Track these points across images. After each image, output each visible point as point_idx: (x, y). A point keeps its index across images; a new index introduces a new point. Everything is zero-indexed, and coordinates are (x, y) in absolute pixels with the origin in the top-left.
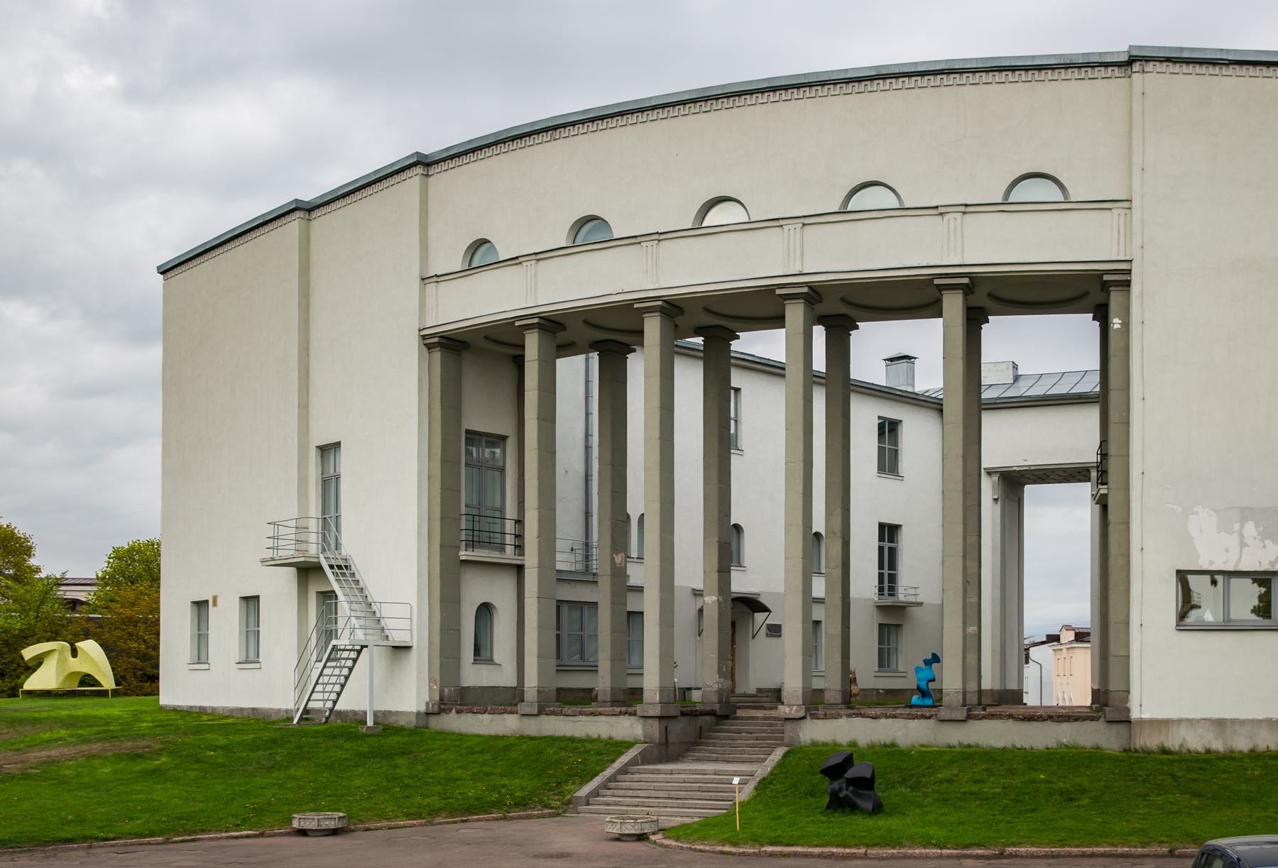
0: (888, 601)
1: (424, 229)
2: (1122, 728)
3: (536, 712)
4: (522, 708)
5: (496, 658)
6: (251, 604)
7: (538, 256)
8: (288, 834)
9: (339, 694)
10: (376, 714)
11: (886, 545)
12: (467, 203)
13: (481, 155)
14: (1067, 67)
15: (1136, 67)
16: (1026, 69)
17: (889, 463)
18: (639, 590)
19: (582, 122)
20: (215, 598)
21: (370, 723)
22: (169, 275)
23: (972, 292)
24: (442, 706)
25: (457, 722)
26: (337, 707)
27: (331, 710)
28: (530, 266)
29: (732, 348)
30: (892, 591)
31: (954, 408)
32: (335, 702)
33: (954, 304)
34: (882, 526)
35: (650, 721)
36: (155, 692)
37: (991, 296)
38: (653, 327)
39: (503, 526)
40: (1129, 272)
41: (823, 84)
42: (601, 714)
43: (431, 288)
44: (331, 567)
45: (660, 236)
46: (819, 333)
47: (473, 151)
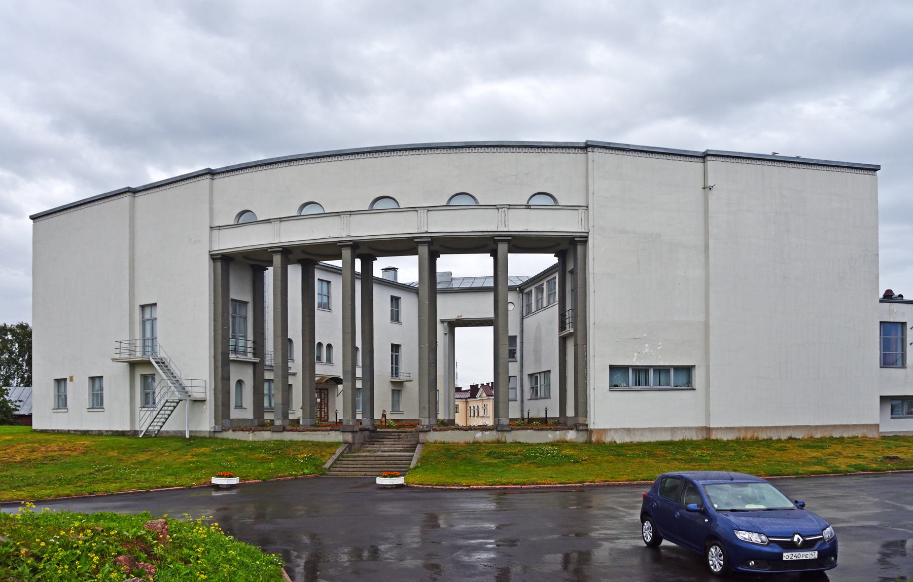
0: (396, 380)
1: (211, 202)
5: (244, 405)
7: (281, 220)
10: (191, 432)
11: (394, 354)
12: (233, 194)
14: (557, 147)
15: (590, 149)
16: (538, 147)
17: (395, 317)
18: (294, 374)
19: (307, 159)
20: (71, 379)
22: (43, 222)
25: (230, 435)
28: (276, 224)
30: (397, 375)
31: (425, 292)
33: (424, 250)
34: (392, 345)
36: (31, 425)
38: (277, 259)
39: (246, 344)
40: (587, 237)
41: (437, 148)
43: (216, 232)
44: (157, 363)
45: (351, 213)
47: (242, 169)
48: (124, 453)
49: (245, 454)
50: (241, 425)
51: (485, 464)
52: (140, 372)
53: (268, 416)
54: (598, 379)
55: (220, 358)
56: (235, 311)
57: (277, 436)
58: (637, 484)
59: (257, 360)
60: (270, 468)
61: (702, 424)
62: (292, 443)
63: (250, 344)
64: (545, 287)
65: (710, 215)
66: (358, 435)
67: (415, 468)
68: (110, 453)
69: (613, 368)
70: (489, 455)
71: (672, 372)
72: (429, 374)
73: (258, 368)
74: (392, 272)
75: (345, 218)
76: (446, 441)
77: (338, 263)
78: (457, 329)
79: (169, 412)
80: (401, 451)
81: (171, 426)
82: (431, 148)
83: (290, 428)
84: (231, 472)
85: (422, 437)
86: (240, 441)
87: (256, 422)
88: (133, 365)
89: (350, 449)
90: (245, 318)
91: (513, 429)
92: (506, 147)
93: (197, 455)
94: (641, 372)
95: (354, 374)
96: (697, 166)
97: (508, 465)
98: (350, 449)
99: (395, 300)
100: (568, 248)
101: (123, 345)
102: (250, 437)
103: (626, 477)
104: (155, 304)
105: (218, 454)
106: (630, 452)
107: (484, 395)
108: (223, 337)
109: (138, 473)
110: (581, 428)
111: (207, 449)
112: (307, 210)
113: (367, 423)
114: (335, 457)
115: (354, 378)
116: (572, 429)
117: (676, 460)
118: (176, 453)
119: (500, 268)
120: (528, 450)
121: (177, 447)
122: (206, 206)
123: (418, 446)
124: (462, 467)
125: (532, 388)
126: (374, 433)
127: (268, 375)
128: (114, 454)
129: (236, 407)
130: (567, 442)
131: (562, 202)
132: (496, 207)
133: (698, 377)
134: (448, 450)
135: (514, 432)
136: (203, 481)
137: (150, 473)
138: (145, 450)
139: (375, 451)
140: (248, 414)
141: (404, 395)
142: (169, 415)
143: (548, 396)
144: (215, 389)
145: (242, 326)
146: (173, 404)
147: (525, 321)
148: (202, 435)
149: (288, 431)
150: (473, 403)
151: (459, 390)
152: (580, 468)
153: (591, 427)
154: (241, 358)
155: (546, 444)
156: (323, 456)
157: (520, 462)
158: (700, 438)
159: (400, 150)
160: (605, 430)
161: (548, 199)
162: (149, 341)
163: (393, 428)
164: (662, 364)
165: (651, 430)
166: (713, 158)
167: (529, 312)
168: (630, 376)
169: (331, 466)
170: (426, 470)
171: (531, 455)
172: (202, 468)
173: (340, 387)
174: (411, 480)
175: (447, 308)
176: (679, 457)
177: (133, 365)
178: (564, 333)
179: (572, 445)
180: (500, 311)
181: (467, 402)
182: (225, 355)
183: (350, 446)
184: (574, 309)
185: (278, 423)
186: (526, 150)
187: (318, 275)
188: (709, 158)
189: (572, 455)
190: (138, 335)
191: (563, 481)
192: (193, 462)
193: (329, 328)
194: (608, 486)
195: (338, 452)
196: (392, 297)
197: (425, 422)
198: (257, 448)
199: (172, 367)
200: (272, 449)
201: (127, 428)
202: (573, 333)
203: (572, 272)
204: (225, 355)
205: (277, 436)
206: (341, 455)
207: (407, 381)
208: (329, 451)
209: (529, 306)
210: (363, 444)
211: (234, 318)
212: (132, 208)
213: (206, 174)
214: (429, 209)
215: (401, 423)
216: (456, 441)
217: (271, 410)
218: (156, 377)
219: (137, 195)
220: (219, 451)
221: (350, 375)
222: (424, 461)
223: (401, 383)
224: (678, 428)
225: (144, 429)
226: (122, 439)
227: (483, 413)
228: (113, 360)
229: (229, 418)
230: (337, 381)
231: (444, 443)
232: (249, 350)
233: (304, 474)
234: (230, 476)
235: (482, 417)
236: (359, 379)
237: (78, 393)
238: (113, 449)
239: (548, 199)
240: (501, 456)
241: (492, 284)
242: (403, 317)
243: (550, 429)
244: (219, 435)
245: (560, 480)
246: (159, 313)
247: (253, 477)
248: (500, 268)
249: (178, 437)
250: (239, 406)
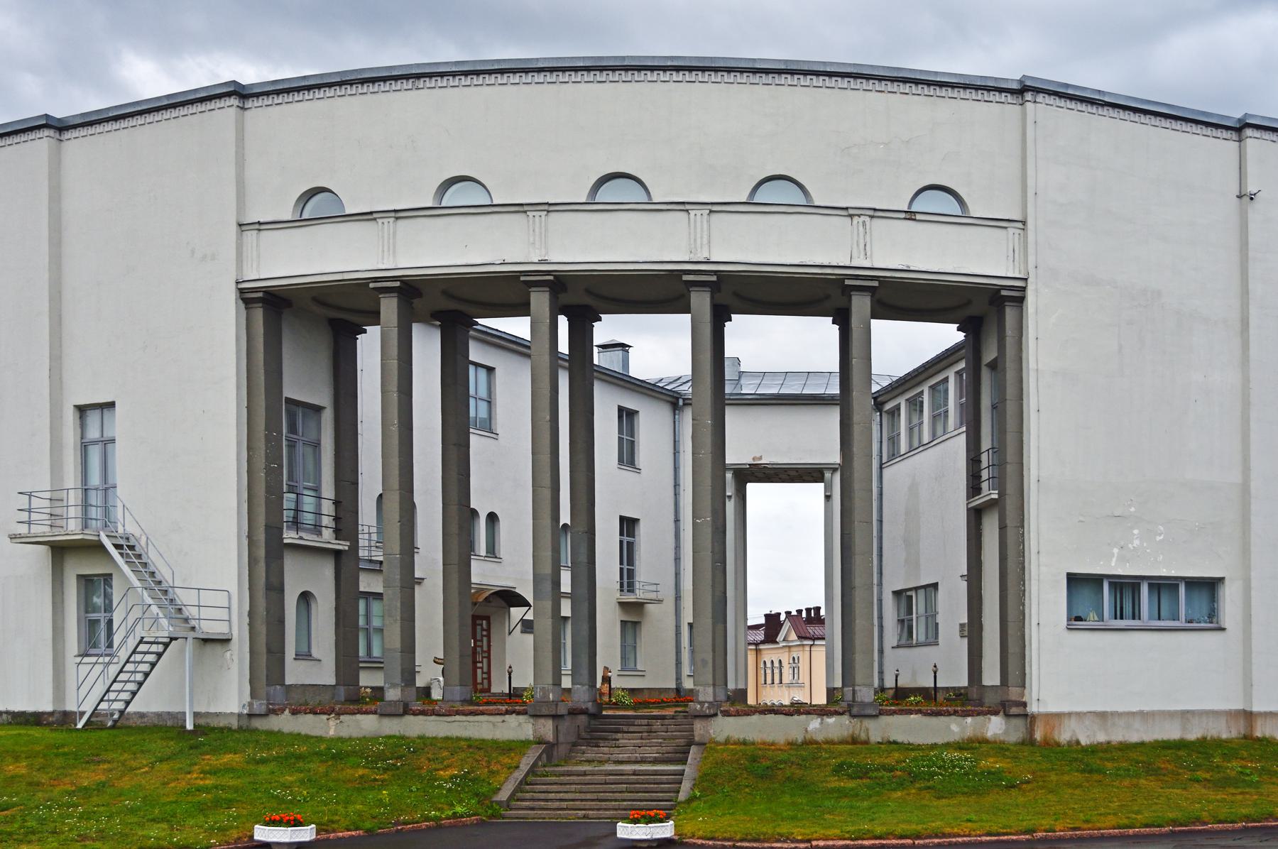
0: (630, 598)
5: (315, 653)
7: (398, 214)
9: (134, 694)
10: (196, 715)
11: (626, 539)
12: (291, 146)
13: (319, 94)
14: (966, 87)
15: (1028, 96)
17: (628, 457)
23: (719, 291)
25: (285, 723)
27: (122, 712)
30: (631, 589)
32: (128, 703)
33: (702, 301)
34: (622, 519)
35: (542, 721)
37: (736, 294)
38: (389, 307)
39: (319, 506)
40: (1024, 289)
41: (729, 70)
42: (482, 713)
43: (251, 236)
44: (117, 547)
45: (549, 207)
46: (563, 322)
48: (41, 769)
49: (322, 769)
50: (308, 701)
51: (832, 791)
52: (75, 568)
53: (368, 680)
54: (1046, 603)
55: (261, 536)
56: (293, 428)
57: (392, 727)
58: (1136, 836)
59: (343, 546)
60: (380, 803)
61: (1239, 706)
62: (426, 742)
63: (328, 508)
64: (926, 398)
65: (1251, 254)
66: (565, 725)
67: (691, 800)
68: (11, 768)
69: (1074, 580)
70: (838, 770)
71: (1145, 589)
72: (713, 586)
73: (345, 564)
74: (618, 353)
75: (538, 217)
76: (407, 734)
77: (519, 327)
78: (750, 486)
79: (146, 667)
80: (655, 761)
81: (149, 702)
82: (716, 70)
83: (417, 706)
84: (295, 812)
85: (698, 726)
86: (308, 737)
87: (342, 692)
88: (60, 551)
89: (550, 758)
90: (316, 445)
91: (881, 713)
92: (868, 77)
93: (214, 772)
94: (1126, 587)
95: (557, 583)
96: (1225, 147)
97: (878, 794)
98: (550, 758)
99: (627, 417)
100: (983, 311)
101: (36, 503)
102: (329, 727)
103: (1111, 820)
104: (111, 405)
105: (262, 768)
106: (1109, 765)
107: (793, 636)
108: (269, 490)
109: (81, 818)
110: (1014, 710)
111: (237, 758)
112: (455, 195)
113: (582, 697)
114: (519, 775)
115: (557, 595)
116: (996, 713)
117: (1198, 781)
118: (165, 767)
119: (852, 352)
120: (915, 759)
121: (168, 751)
122: (230, 172)
123: (693, 749)
124: (787, 798)
125: (901, 622)
126: (596, 719)
127: (368, 583)
128: (21, 768)
129: (299, 656)
130: (986, 741)
131: (976, 210)
132: (848, 212)
133: (1230, 598)
134: (754, 759)
135: (885, 719)
136: (234, 834)
137: (110, 817)
138: (93, 759)
139: (601, 762)
140: (324, 673)
141: (646, 631)
142: (147, 675)
143: (932, 639)
144: (251, 614)
145: (310, 466)
146: (154, 648)
147: (885, 472)
148: (223, 723)
149: (415, 714)
150: (771, 654)
152: (1021, 800)
154: (309, 539)
155: (947, 746)
156: (492, 772)
157: (901, 785)
158: (1234, 734)
159: (652, 69)
160: (1059, 716)
161: (941, 201)
162: (98, 493)
163: (626, 707)
164: (1164, 572)
166: (1257, 134)
167: (894, 454)
168: (1109, 598)
169: (513, 794)
170: (713, 806)
171: (919, 772)
172: (230, 804)
173: (517, 613)
174: (688, 829)
175: (746, 439)
176: (1201, 774)
177: (60, 551)
178: (978, 501)
179: (999, 748)
180: (857, 448)
181: (758, 651)
182: (274, 531)
183: (550, 748)
184: (999, 450)
185: (393, 694)
186: (906, 88)
187: (476, 353)
188: (1249, 132)
189: (999, 771)
190: (71, 478)
191: (995, 829)
192: (207, 790)
193: (503, 474)
194: (1081, 839)
195: (526, 763)
196: (621, 410)
197: (706, 694)
198: (348, 754)
199: (153, 557)
200: (381, 757)
201: (45, 705)
202: (995, 497)
203: (993, 366)
204: (274, 531)
205: (392, 727)
206: (532, 771)
207: (652, 601)
208: (507, 760)
209: (894, 440)
210: (574, 745)
211: (292, 445)
213: (228, 95)
214: (714, 208)
215: (640, 698)
216: (769, 739)
217: (376, 665)
218: (115, 582)
219: (67, 135)
220: (263, 761)
221: (548, 586)
222: (706, 782)
223: (638, 607)
224: (1192, 713)
225: (88, 708)
226: (36, 732)
227: (808, 674)
228: (13, 537)
229: (283, 684)
230: (510, 598)
231: (744, 743)
232: (326, 521)
233: (455, 815)
234: (296, 823)
235: (789, 685)
236: (566, 595)
238: (17, 758)
239: (941, 201)
240: (862, 773)
241: (835, 390)
242: (642, 457)
243: (955, 713)
244: (258, 724)
245: (987, 827)
246: (119, 425)
247: (344, 823)
248: (852, 352)
249: (167, 728)
250: (304, 655)
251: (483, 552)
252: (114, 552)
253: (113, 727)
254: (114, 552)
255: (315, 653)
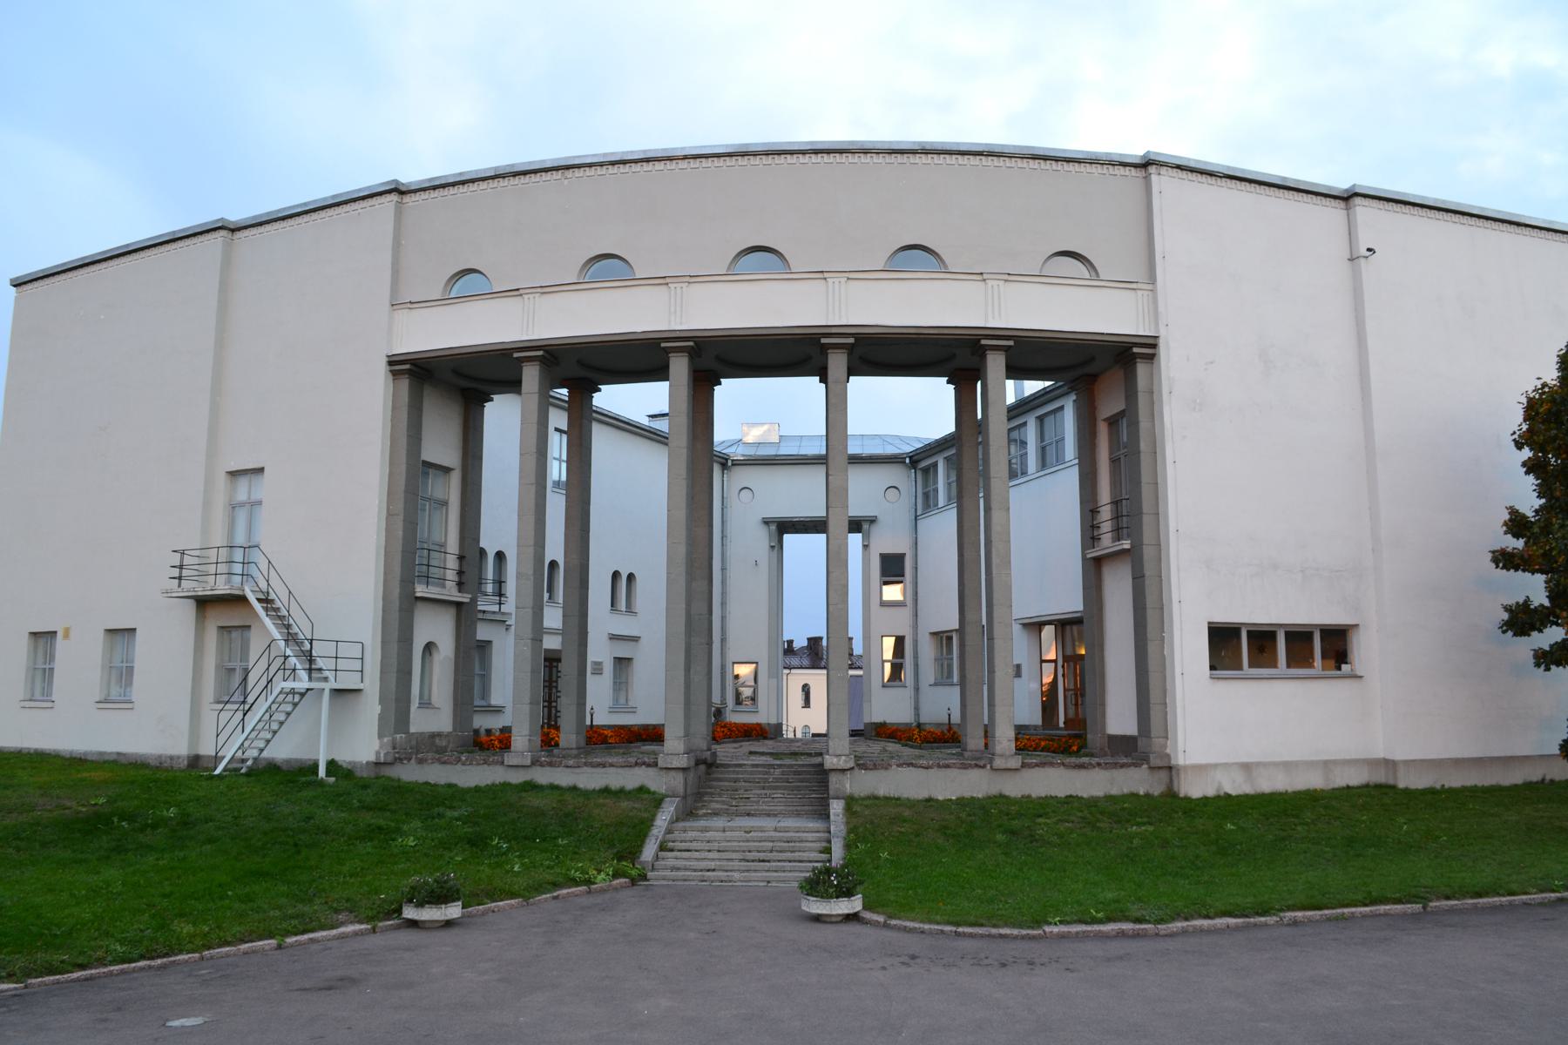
2: (1163, 775)
3: (528, 762)
4: (510, 759)
6: (42, 642)
8: (398, 927)
15: (1152, 169)
21: (322, 772)
24: (400, 756)
25: (410, 773)
26: (265, 754)
27: (255, 759)
29: (595, 402)
32: (262, 750)
35: (673, 773)
40: (1154, 346)
50: (429, 748)
54: (1188, 649)
59: (465, 598)
66: (691, 775)
81: (283, 750)
94: (1262, 639)
104: (261, 470)
149: (542, 765)
151: (789, 650)
153: (1181, 760)
165: (1287, 766)
177: (204, 603)
178: (1092, 554)
188: (1358, 200)
203: (1113, 422)
204: (407, 582)
212: (227, 263)
229: (407, 732)
237: (81, 661)
251: (623, 608)
252: (258, 607)
253: (248, 774)
254: (258, 607)
255: (435, 700)
